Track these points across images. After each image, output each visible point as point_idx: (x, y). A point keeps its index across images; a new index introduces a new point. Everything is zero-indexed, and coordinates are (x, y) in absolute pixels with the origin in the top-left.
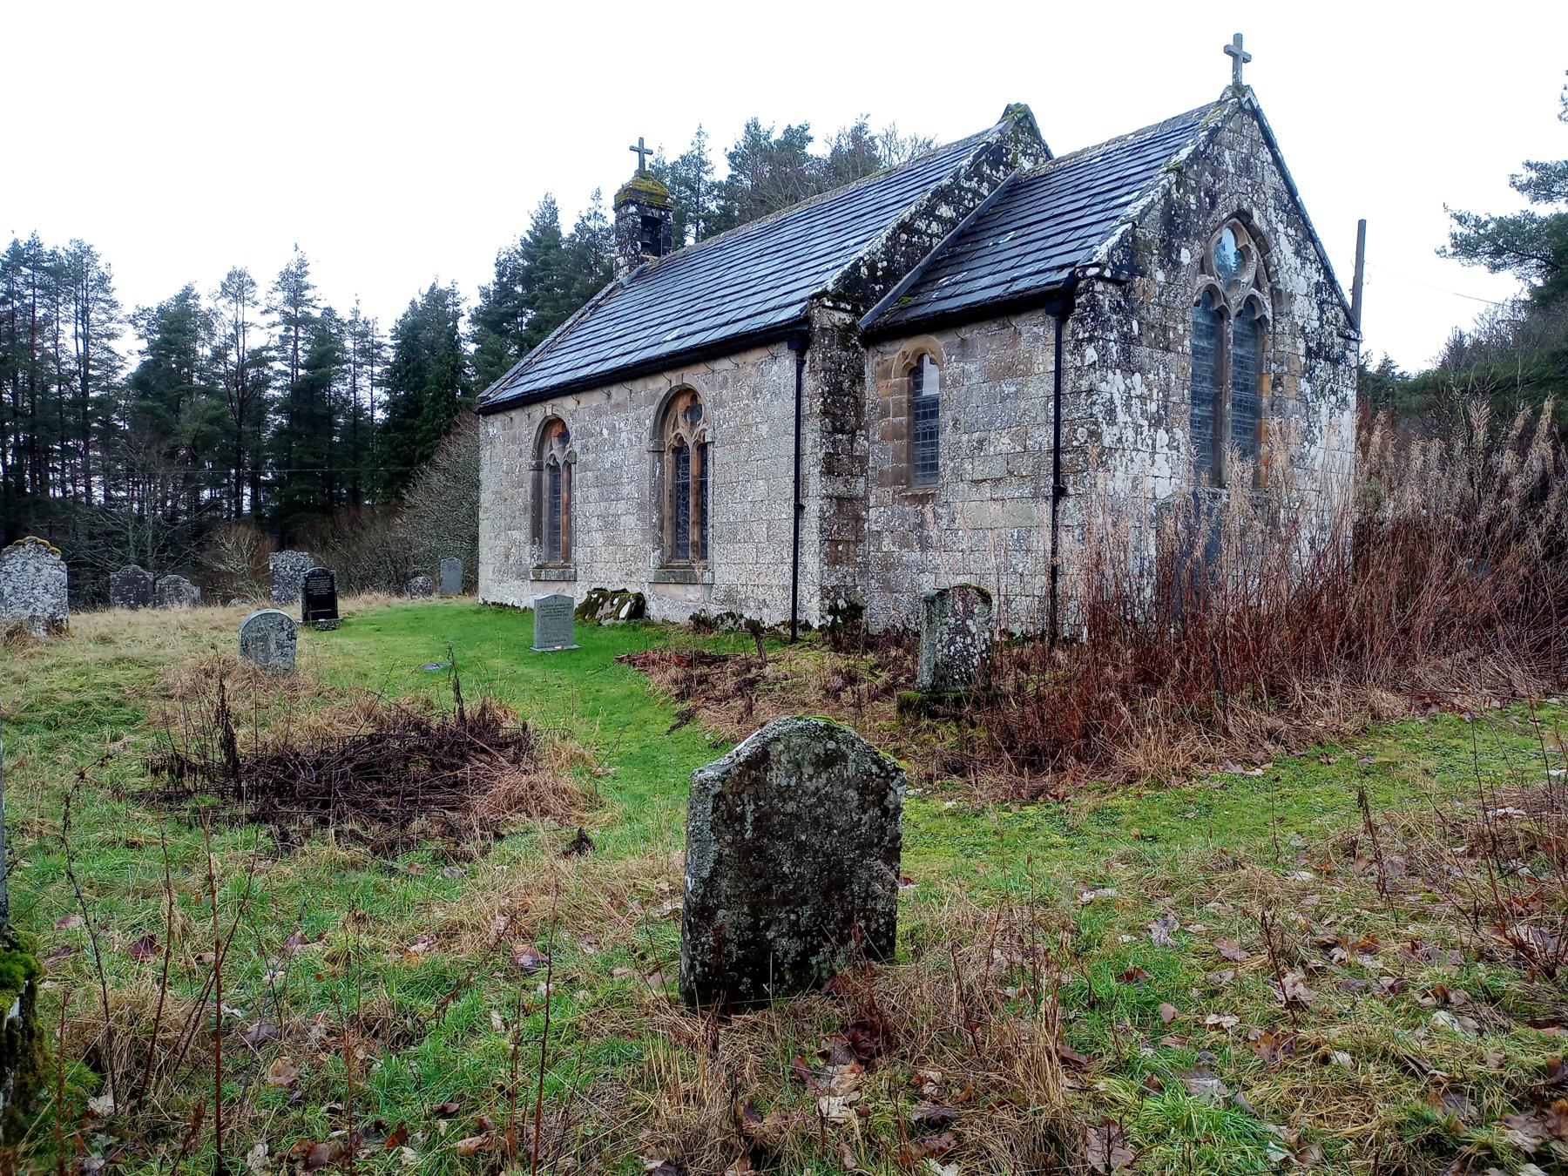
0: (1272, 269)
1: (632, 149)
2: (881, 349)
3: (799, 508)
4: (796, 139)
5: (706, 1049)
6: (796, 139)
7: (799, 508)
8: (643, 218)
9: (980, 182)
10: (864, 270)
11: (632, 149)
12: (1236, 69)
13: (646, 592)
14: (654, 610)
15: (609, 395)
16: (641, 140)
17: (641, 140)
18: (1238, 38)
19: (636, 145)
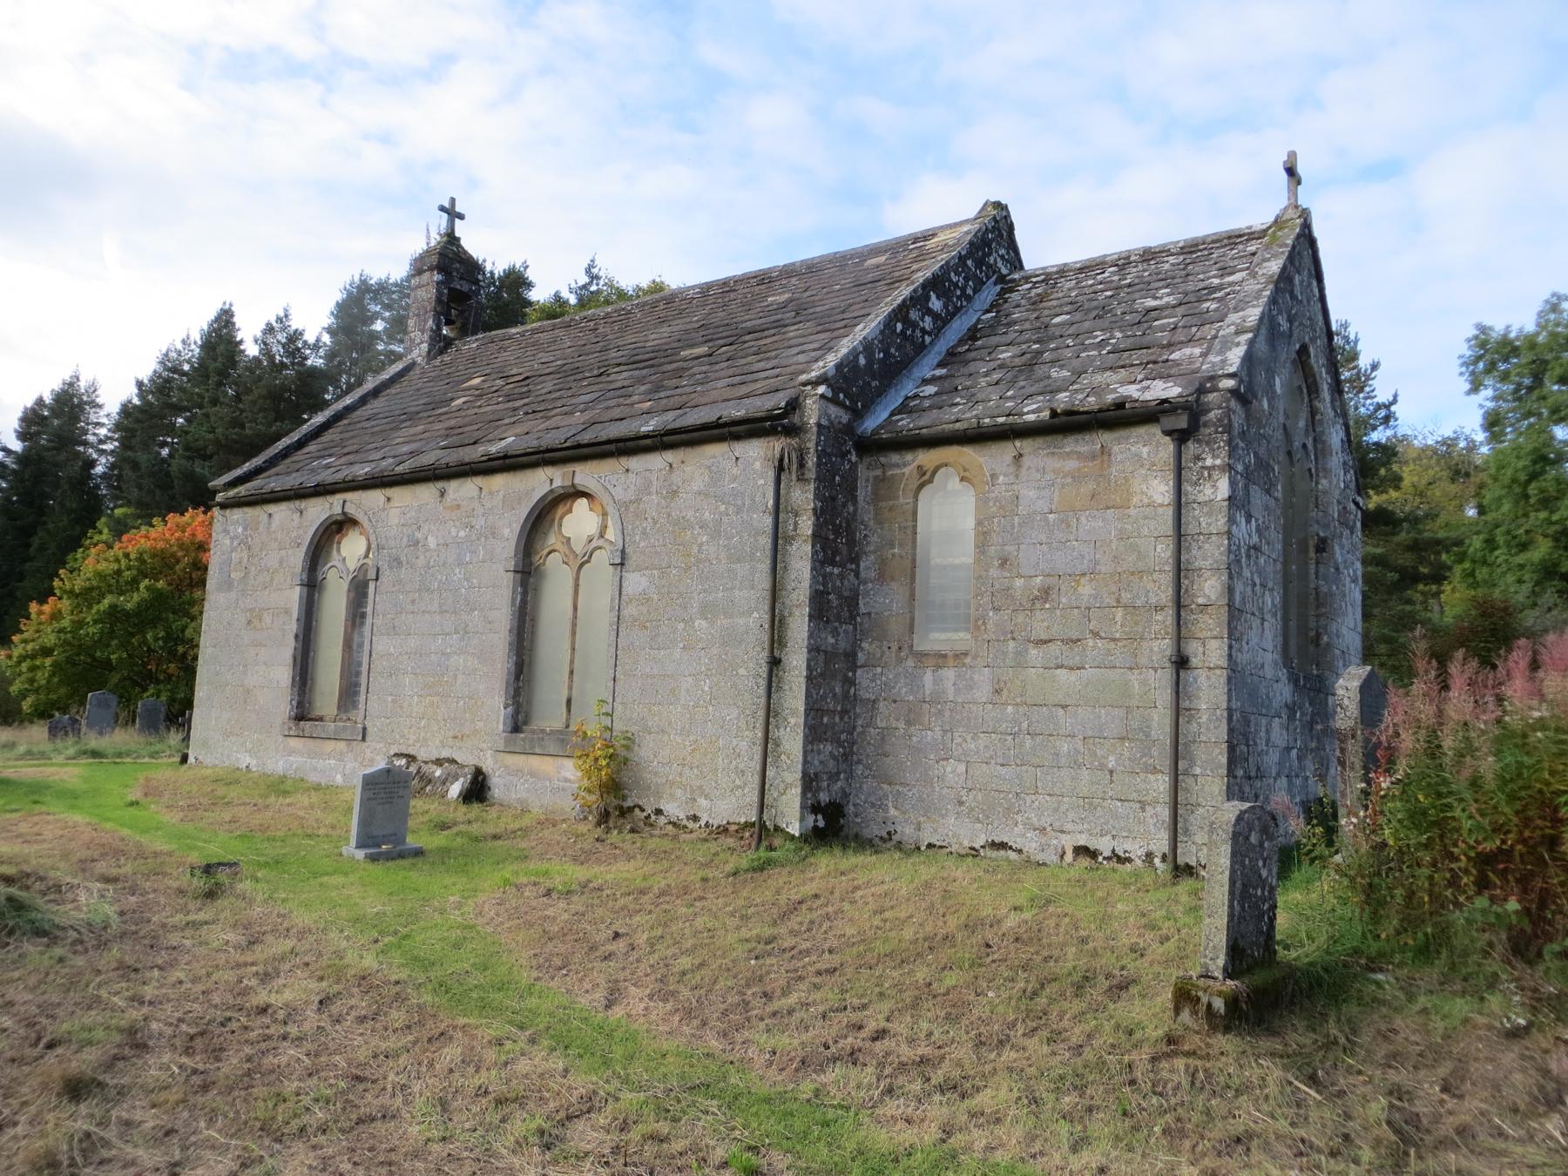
0: (1318, 417)
1: (442, 209)
2: (882, 460)
3: (775, 663)
4: (529, 285)
5: (175, 954)
6: (529, 285)
7: (775, 663)
8: (450, 289)
9: (966, 279)
10: (862, 361)
11: (442, 209)
12: (1293, 193)
13: (488, 765)
14: (498, 787)
15: (442, 494)
16: (453, 201)
17: (453, 201)
18: (1292, 155)
19: (447, 205)
